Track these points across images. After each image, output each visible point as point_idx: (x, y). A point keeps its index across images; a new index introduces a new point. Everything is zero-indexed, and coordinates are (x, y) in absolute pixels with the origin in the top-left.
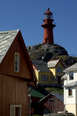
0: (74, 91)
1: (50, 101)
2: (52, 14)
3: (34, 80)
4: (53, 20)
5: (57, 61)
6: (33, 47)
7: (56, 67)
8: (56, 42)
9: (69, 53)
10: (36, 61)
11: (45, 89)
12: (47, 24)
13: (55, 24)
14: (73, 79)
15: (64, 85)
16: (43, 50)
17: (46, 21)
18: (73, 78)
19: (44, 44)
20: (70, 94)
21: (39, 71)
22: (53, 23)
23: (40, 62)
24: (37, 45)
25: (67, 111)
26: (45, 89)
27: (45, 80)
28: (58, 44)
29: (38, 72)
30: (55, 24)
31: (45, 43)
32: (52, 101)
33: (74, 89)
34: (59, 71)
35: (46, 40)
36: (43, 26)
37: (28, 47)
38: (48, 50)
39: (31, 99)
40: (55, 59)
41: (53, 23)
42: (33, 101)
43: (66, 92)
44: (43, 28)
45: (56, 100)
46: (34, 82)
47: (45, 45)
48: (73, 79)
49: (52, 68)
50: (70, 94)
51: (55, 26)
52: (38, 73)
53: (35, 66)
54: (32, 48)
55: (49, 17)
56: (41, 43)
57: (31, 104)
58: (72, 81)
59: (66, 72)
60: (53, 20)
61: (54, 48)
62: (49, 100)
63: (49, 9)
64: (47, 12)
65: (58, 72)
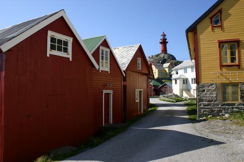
0: (178, 81)
22: (167, 41)
35: (163, 51)
36: (160, 43)
38: (164, 57)
41: (167, 41)
43: (174, 82)
56: (160, 53)
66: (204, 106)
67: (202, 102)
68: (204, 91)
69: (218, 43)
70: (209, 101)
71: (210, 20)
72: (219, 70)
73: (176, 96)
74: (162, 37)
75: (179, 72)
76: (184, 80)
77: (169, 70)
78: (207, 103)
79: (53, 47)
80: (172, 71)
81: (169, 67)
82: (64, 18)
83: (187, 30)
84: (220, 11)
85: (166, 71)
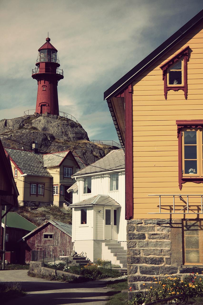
0: (90, 214)
1: (46, 236)
2: (57, 51)
3: (13, 193)
4: (59, 65)
5: (64, 154)
6: (13, 122)
7: (62, 166)
8: (64, 113)
9: (114, 97)
10: (19, 153)
11: (172, 62)
12: (43, 71)
13: (63, 73)
14: (91, 193)
15: (72, 203)
16: (35, 128)
17: (43, 66)
18: (91, 191)
19: (37, 115)
20: (84, 220)
21: (25, 174)
22: (59, 71)
23: (27, 156)
24: (21, 118)
25: (76, 252)
26: (62, 150)
27: (37, 186)
28: (68, 115)
29: (24, 176)
30: (61, 74)
31: (39, 112)
32: (51, 236)
33: (91, 210)
34: (68, 169)
35: (42, 106)
36: (34, 77)
37: (3, 120)
38: (44, 129)
39: (6, 233)
40: (60, 149)
41: (59, 71)
42: (9, 238)
43: (77, 215)
44: (36, 81)
45: (59, 235)
46: (12, 196)
47: (41, 118)
48: (91, 193)
49: (51, 168)
50: (84, 220)
51: (61, 77)
52: (22, 179)
53: (15, 163)
54: (10, 123)
55: (50, 59)
56: (32, 113)
57: (6, 243)
58: (88, 196)
59: (77, 178)
60: (59, 65)
61: (58, 126)
62: (44, 234)
63: (48, 40)
64: (46, 47)
65: (66, 176)
66: (142, 272)
67: (138, 262)
68: (143, 237)
69: (176, 128)
70: (153, 261)
71: (161, 72)
72: (178, 188)
73: (82, 260)
74: (44, 57)
75: (95, 183)
76: (108, 213)
77: (63, 175)
78: (149, 266)
79: (42, 186)
80: (74, 181)
81: (62, 166)
82: (54, 178)
83: (104, 93)
84: (188, 51)
85: (51, 179)
